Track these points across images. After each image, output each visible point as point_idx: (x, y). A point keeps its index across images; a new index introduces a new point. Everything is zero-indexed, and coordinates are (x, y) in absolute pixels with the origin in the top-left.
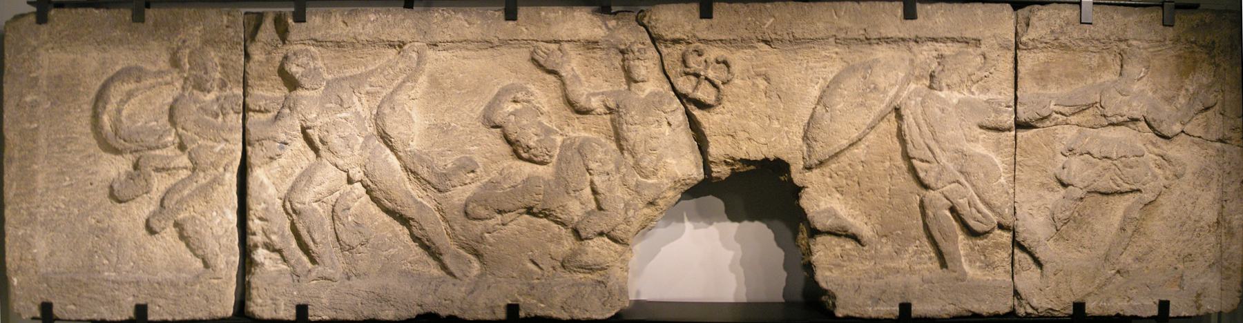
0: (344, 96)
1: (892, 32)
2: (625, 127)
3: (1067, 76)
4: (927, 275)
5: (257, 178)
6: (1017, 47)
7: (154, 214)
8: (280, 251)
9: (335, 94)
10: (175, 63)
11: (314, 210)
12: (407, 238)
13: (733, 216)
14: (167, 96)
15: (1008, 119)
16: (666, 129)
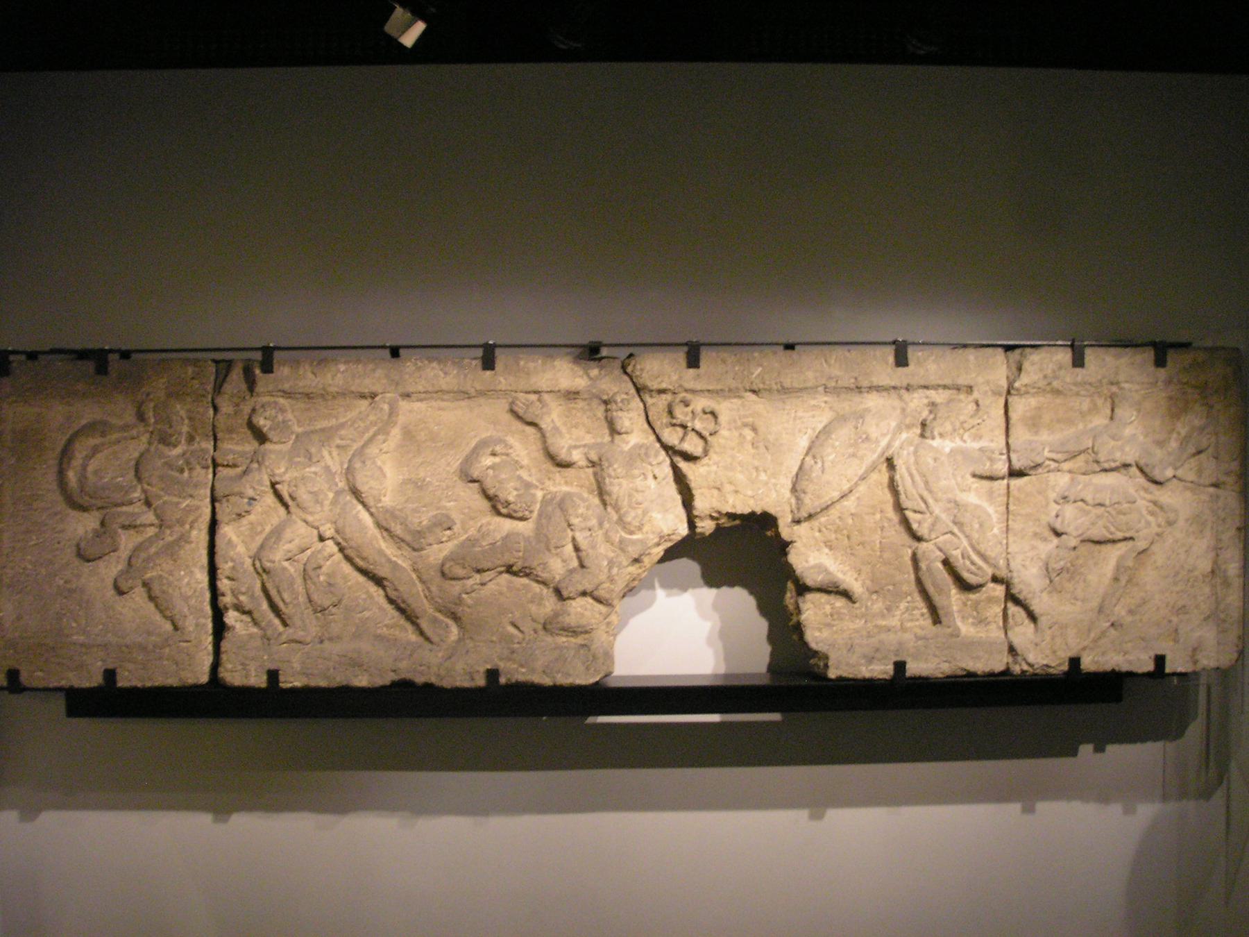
0: (313, 450)
1: (885, 381)
2: (607, 481)
3: (1059, 421)
4: (920, 632)
5: (225, 535)
6: (1009, 392)
7: (122, 573)
8: (249, 613)
9: (303, 450)
10: (141, 417)
11: (284, 569)
12: (382, 601)
13: (712, 579)
14: (133, 451)
15: (1002, 468)
16: (651, 482)
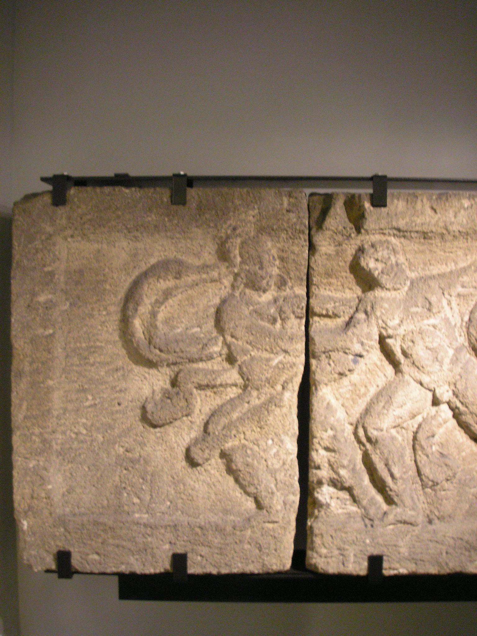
0: (433, 299)
7: (196, 441)
8: (349, 490)
10: (223, 255)
11: (393, 438)
14: (213, 296)
